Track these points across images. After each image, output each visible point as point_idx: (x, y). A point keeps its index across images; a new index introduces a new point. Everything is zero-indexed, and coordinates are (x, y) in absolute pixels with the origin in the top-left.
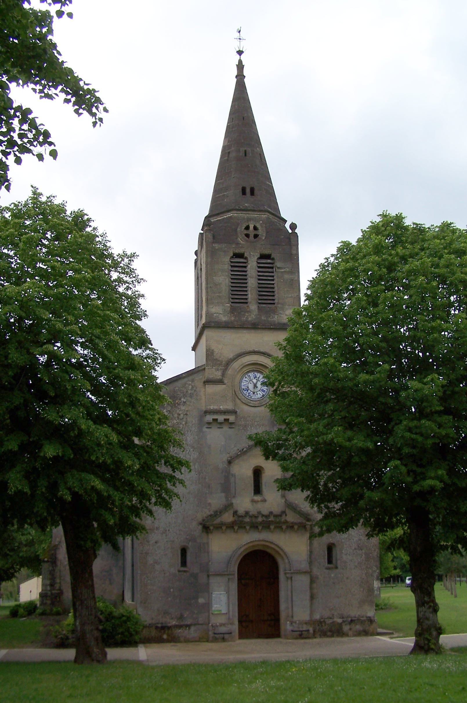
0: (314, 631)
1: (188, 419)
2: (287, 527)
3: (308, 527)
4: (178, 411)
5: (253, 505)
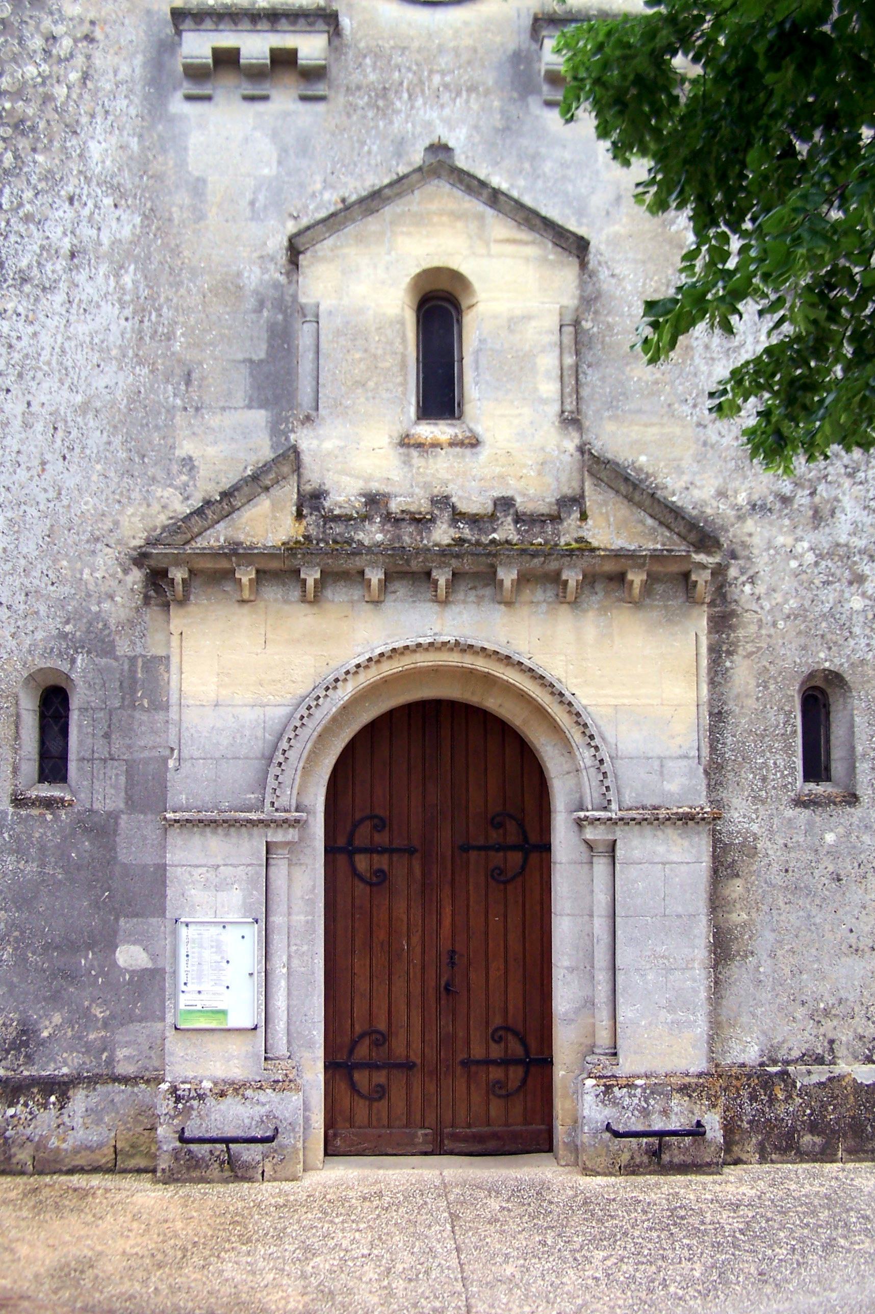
0: (729, 1128)
1: (98, 62)
2: (590, 580)
3: (701, 578)
4: (47, 23)
5: (407, 462)
